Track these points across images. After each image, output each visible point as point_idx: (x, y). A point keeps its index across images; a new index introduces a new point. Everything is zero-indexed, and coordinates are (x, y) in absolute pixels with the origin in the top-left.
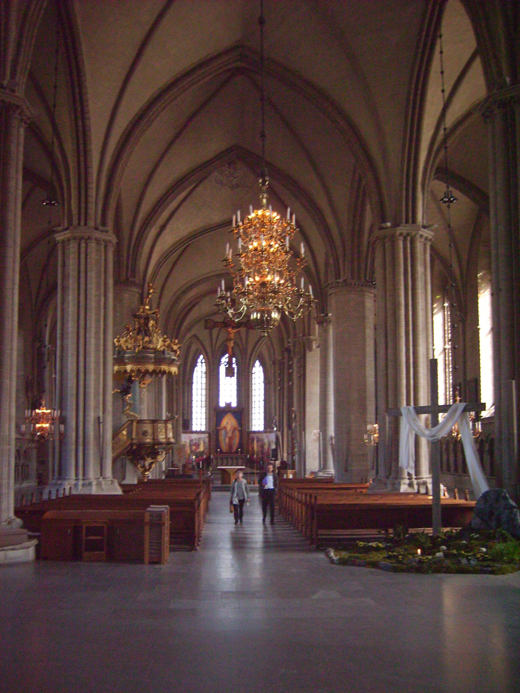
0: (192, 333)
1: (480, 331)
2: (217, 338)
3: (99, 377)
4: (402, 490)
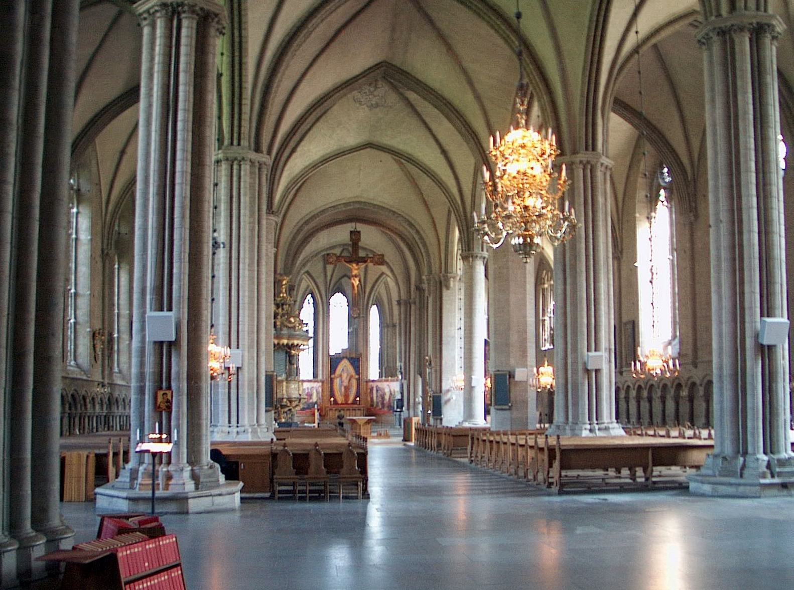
0: (306, 269)
1: (639, 269)
2: (332, 276)
3: (253, 314)
4: (584, 435)
